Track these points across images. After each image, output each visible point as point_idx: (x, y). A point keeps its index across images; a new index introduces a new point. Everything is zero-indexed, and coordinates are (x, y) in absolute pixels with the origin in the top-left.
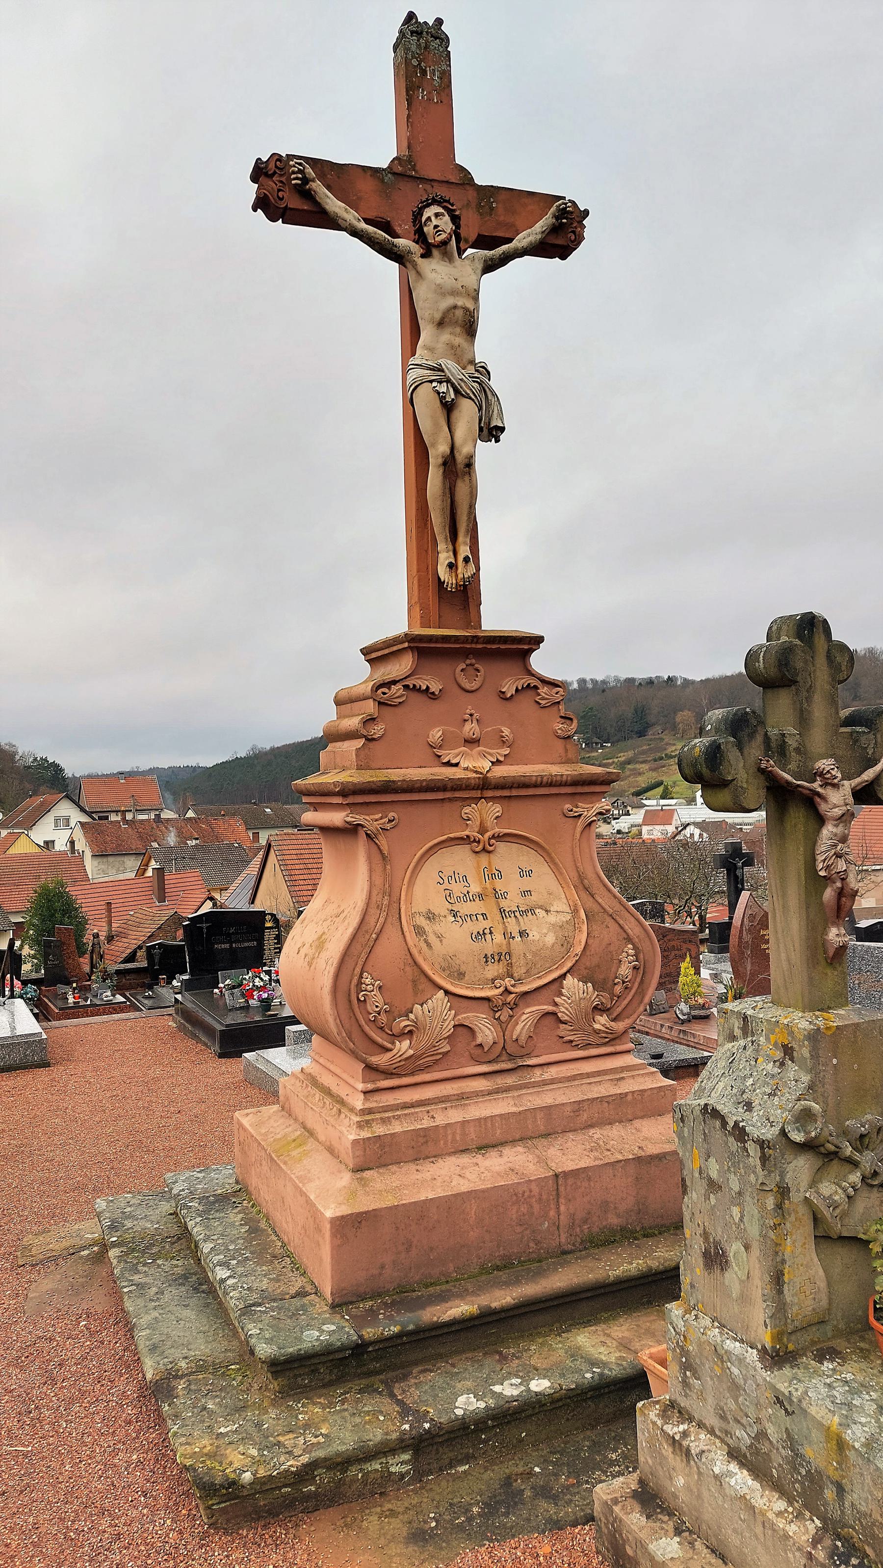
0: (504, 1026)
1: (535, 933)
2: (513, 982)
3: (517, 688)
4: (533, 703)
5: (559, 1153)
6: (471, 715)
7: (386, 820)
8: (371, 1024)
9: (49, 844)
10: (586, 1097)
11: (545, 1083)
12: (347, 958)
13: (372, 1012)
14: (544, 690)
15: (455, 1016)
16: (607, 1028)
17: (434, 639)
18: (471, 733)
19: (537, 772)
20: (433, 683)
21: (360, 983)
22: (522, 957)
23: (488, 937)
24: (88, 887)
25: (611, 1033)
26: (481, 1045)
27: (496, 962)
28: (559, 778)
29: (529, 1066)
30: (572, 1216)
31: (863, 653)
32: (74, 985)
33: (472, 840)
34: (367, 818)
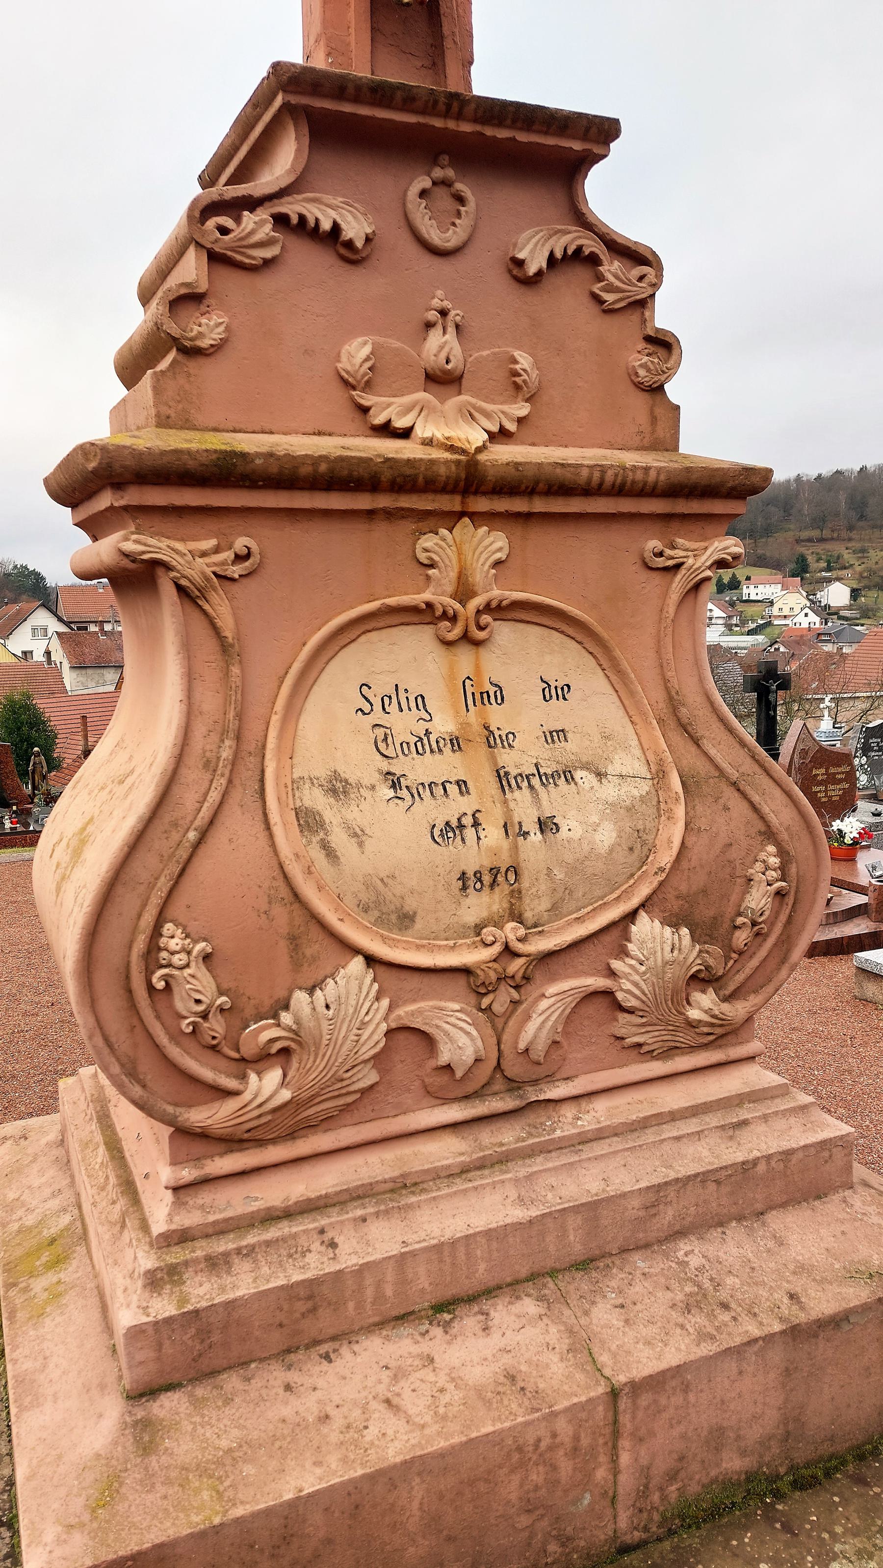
0: (499, 1022)
1: (573, 824)
2: (522, 932)
3: (552, 255)
4: (586, 300)
5: (615, 1319)
6: (444, 313)
7: (228, 555)
8: (186, 1042)
9: (27, 654)
10: (672, 1175)
11: (584, 1140)
12: (120, 890)
13: (185, 1013)
14: (611, 268)
15: (391, 1008)
16: (714, 1016)
17: (351, 90)
18: (443, 356)
19: (590, 459)
20: (350, 218)
21: (153, 947)
22: (543, 877)
23: (470, 833)
24: (64, 699)
25: (721, 1026)
26: (448, 1067)
27: (486, 889)
28: (639, 476)
29: (549, 1101)
30: (645, 1472)
31: (873, 469)
32: (14, 808)
33: (439, 612)
34: (179, 546)
